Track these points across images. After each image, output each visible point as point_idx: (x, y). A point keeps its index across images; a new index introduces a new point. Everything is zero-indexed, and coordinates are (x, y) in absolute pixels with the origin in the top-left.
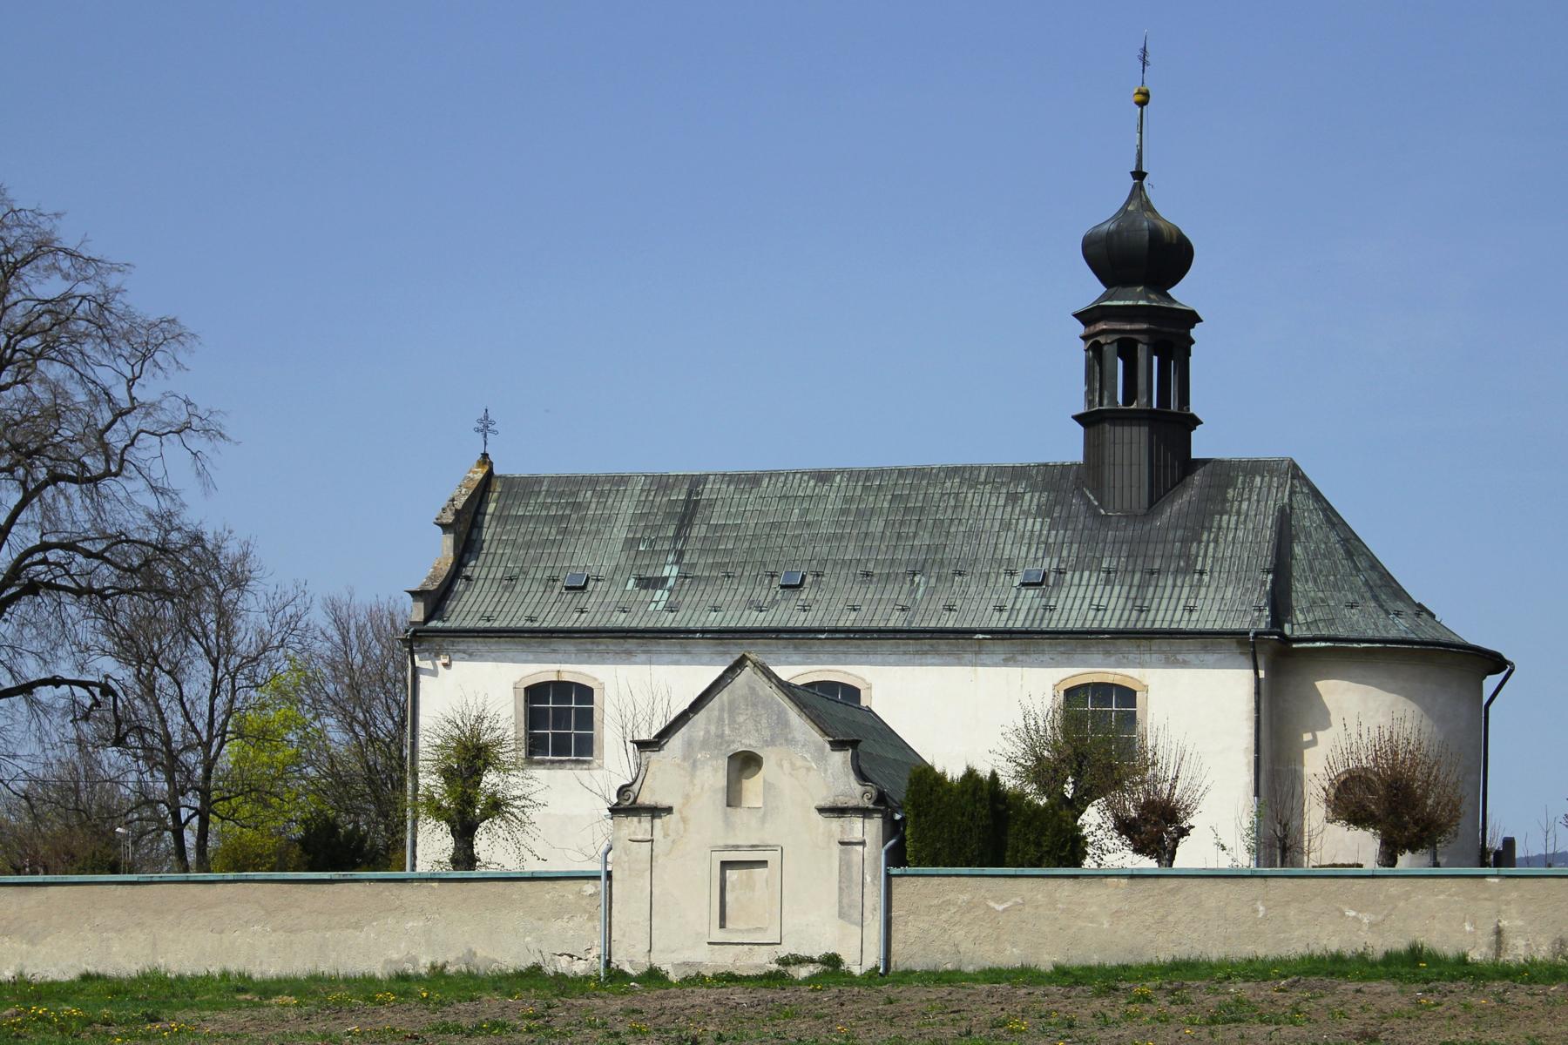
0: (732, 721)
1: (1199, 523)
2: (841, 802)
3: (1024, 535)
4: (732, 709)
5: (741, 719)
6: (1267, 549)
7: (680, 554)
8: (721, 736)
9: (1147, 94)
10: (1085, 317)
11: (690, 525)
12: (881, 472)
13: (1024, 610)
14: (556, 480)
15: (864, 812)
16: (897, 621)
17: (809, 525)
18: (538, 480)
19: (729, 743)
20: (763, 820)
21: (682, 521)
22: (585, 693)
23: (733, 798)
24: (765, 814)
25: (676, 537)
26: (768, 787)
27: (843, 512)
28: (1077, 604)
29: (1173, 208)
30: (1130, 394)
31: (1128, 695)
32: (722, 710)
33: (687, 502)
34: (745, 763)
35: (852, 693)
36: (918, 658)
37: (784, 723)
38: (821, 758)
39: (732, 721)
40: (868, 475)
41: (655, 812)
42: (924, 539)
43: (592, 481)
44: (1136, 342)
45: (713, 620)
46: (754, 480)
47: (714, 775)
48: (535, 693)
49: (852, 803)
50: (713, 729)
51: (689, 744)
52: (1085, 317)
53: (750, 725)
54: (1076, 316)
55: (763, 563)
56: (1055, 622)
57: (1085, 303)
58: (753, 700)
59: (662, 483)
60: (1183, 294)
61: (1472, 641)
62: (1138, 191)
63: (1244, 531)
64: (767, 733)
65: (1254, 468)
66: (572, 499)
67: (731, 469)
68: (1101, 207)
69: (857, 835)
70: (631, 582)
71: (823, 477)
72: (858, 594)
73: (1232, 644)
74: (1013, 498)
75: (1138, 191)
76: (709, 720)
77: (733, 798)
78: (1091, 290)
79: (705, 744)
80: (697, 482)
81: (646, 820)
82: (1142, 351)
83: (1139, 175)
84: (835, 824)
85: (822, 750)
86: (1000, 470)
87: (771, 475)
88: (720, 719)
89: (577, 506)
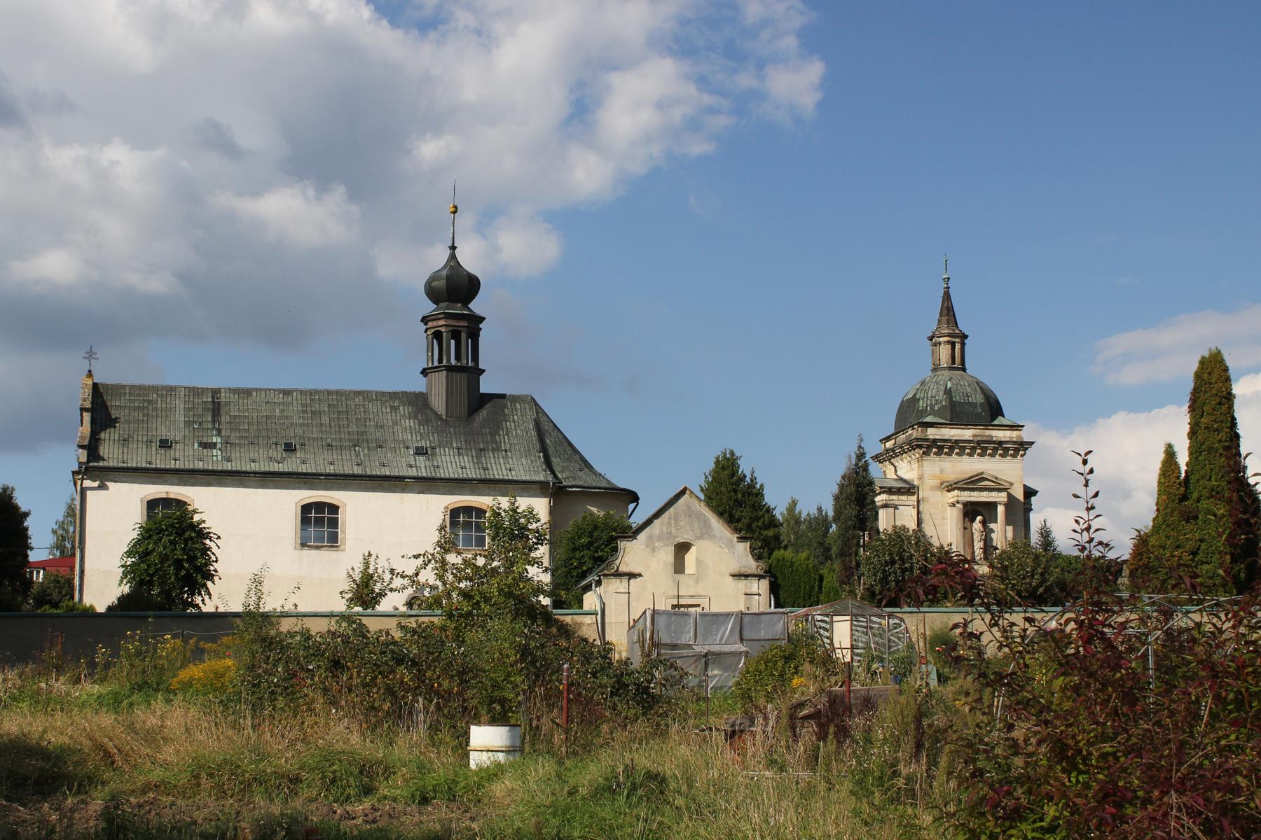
0: (677, 525)
1: (496, 425)
2: (743, 571)
3: (407, 428)
4: (676, 518)
5: (682, 523)
6: (535, 439)
7: (219, 431)
8: (670, 533)
9: (455, 207)
10: (425, 320)
11: (219, 415)
12: (317, 392)
13: (422, 467)
14: (132, 387)
15: (760, 577)
16: (357, 470)
17: (287, 418)
18: (123, 387)
19: (675, 538)
20: (697, 581)
21: (213, 411)
22: (334, 509)
23: (679, 567)
24: (697, 578)
25: (214, 422)
26: (699, 563)
27: (304, 412)
28: (451, 464)
29: (469, 261)
30: (440, 361)
31: (334, 509)
32: (670, 518)
33: (213, 402)
34: (682, 549)
35: (181, 504)
36: (374, 489)
37: (707, 526)
38: (730, 546)
39: (677, 525)
40: (311, 393)
41: (632, 576)
42: (353, 428)
43: (155, 389)
44: (460, 332)
45: (254, 467)
46: (248, 392)
47: (668, 555)
48: (306, 509)
49: (750, 572)
50: (665, 529)
51: (650, 537)
52: (425, 320)
53: (688, 528)
54: (484, 319)
55: (269, 438)
56: (442, 474)
57: (425, 313)
58: (690, 512)
59: (195, 392)
60: (476, 306)
61: (621, 486)
62: (453, 257)
63: (519, 428)
64: (698, 532)
65: (515, 399)
66: (149, 398)
67: (233, 386)
68: (437, 259)
69: (755, 590)
70: (196, 446)
71: (287, 393)
72: (329, 456)
73: (538, 486)
74: (394, 409)
75: (453, 257)
76: (662, 524)
77: (679, 567)
78: (429, 307)
79: (660, 538)
80: (215, 392)
81: (625, 579)
82: (463, 336)
83: (453, 248)
84: (742, 585)
85: (731, 542)
86: (383, 394)
87: (256, 390)
88: (669, 523)
89: (150, 402)
